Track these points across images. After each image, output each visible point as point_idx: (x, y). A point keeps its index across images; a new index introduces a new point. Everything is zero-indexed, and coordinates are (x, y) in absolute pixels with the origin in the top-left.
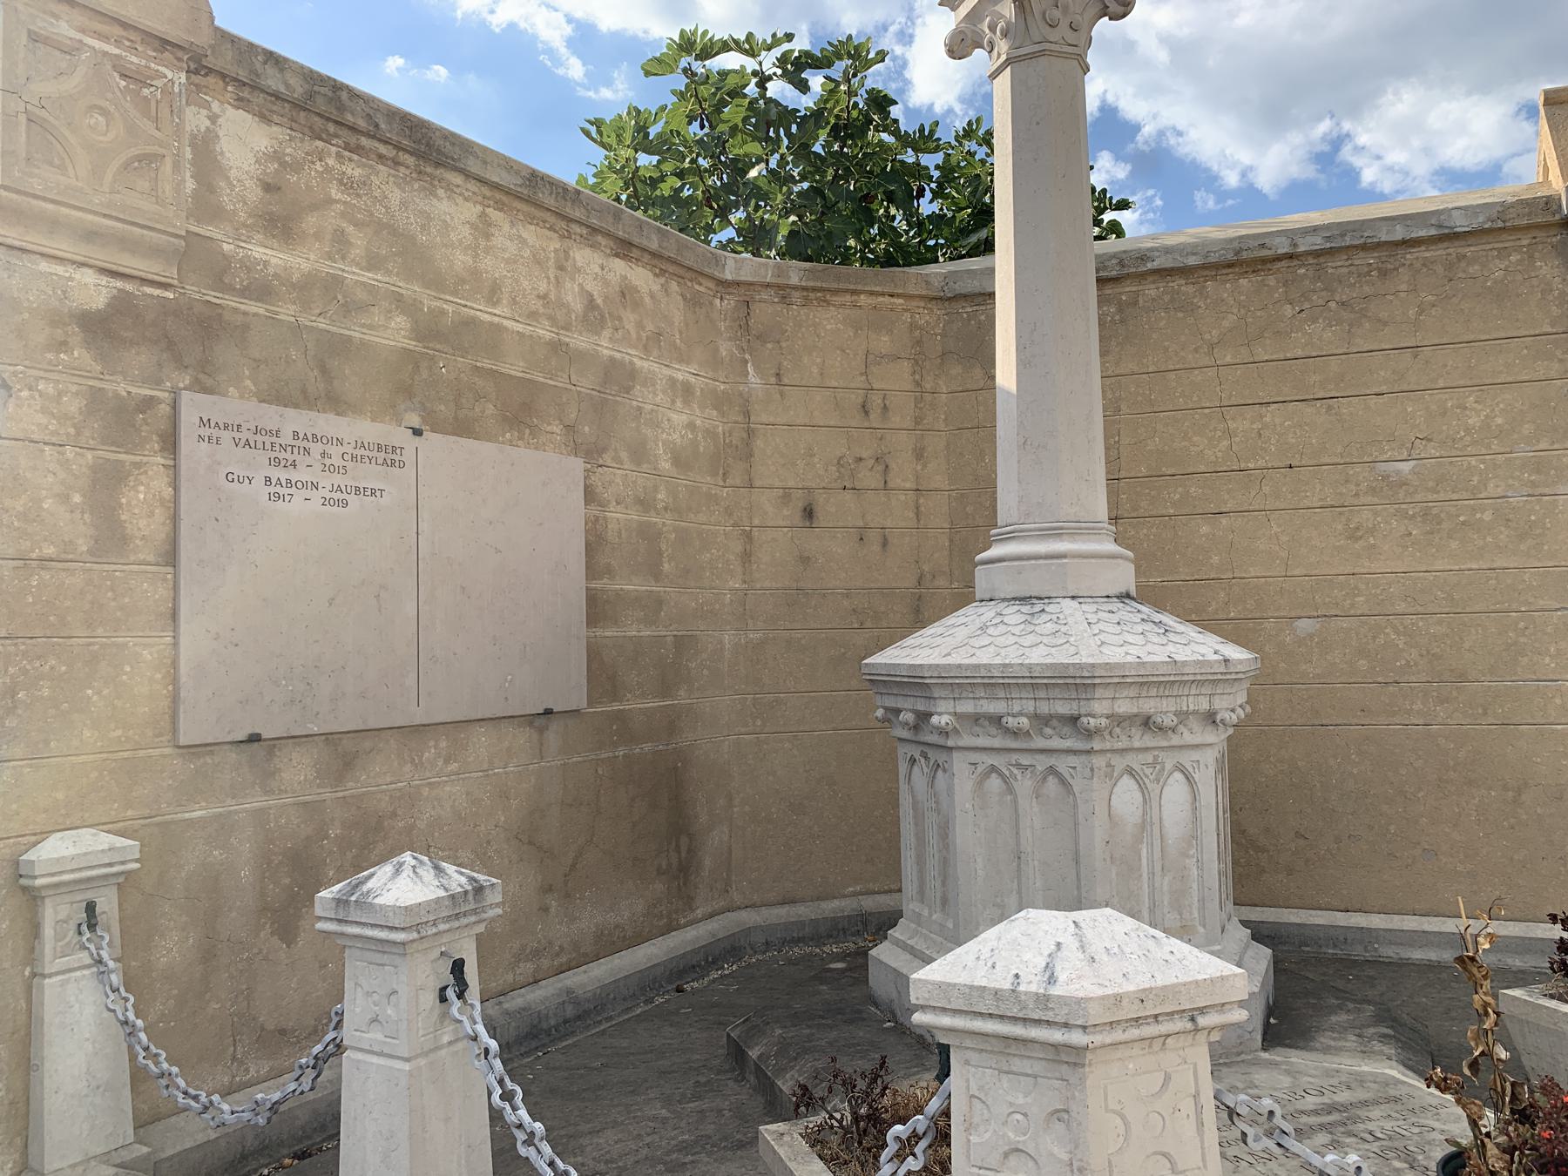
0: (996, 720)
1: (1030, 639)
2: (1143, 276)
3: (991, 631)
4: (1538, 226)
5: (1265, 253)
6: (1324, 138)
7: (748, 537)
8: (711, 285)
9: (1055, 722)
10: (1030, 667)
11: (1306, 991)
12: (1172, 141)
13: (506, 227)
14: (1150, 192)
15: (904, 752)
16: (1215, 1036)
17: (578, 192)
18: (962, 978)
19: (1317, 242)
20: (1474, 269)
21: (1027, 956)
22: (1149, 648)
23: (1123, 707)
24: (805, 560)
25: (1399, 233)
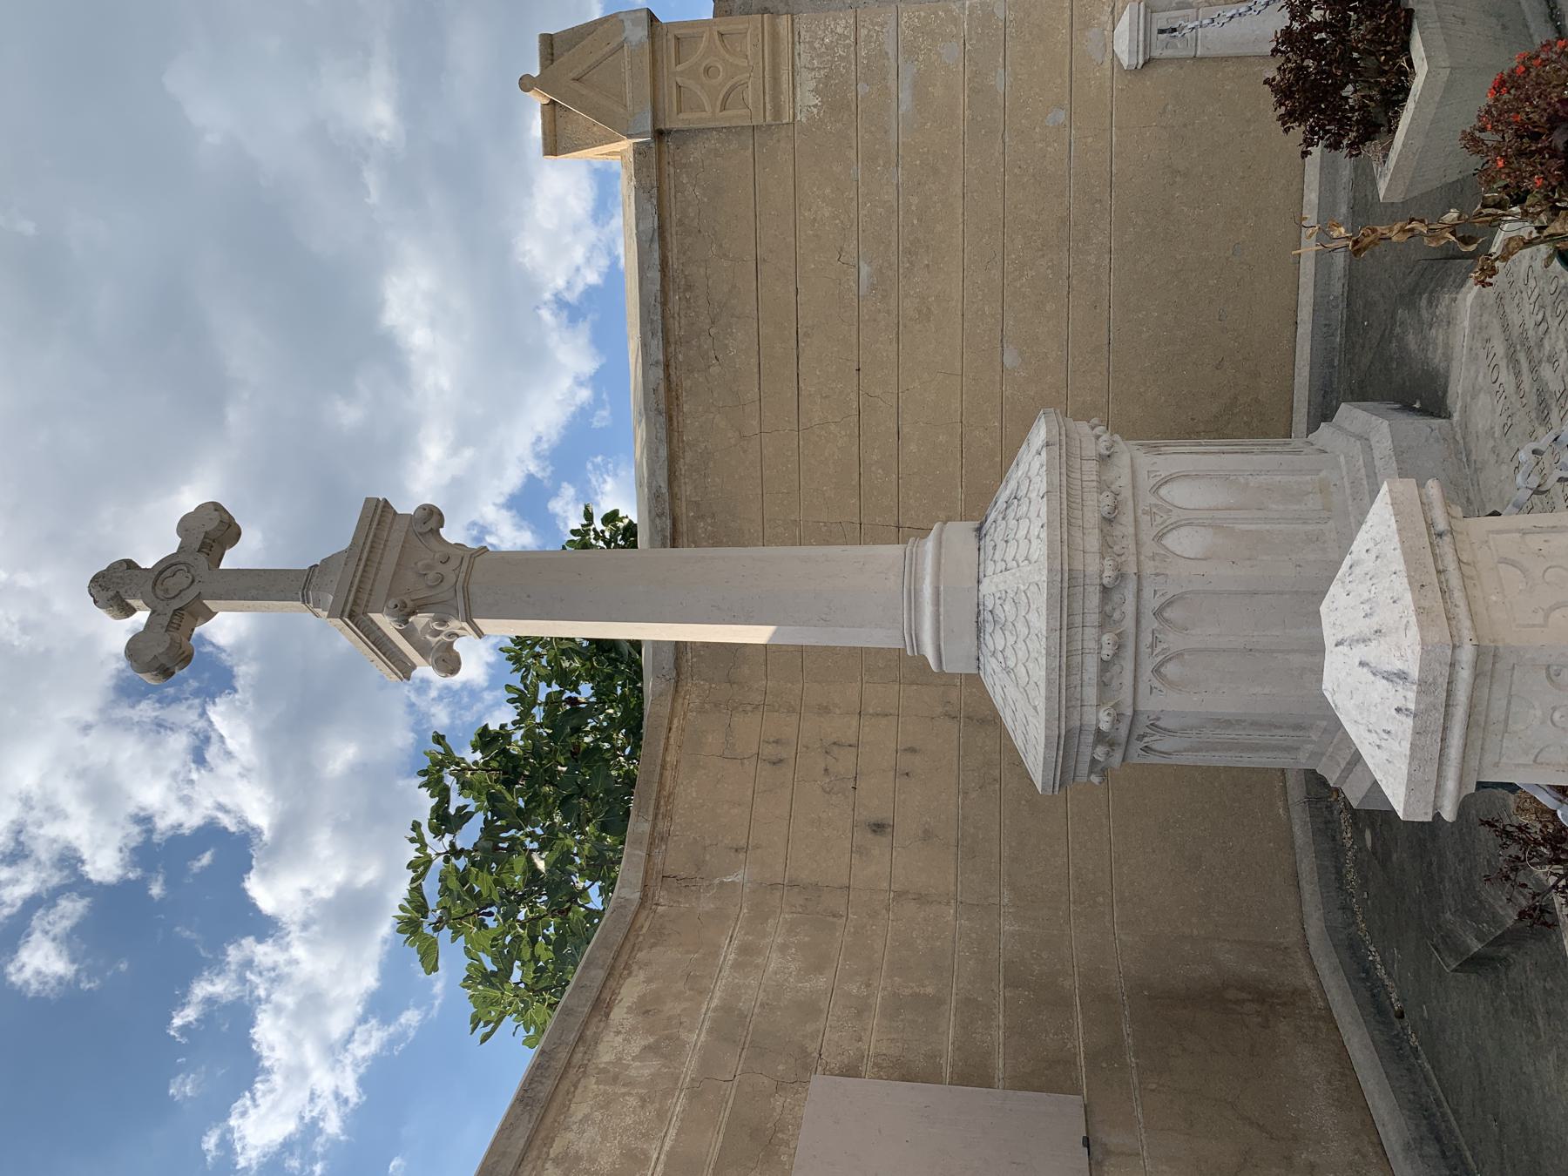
0: (1105, 666)
1: (1023, 630)
2: (673, 496)
3: (1011, 664)
4: (659, 161)
5: (662, 389)
6: (555, 315)
7: (900, 895)
8: (644, 914)
9: (1108, 608)
10: (1050, 630)
11: (1378, 366)
12: (546, 446)
13: (571, 1136)
14: (589, 466)
15: (1136, 756)
16: (1457, 511)
17: (542, 1052)
18: (1403, 767)
19: (656, 344)
20: (692, 212)
21: (1376, 698)
22: (1033, 515)
23: (1093, 542)
24: (927, 835)
25: (655, 274)
